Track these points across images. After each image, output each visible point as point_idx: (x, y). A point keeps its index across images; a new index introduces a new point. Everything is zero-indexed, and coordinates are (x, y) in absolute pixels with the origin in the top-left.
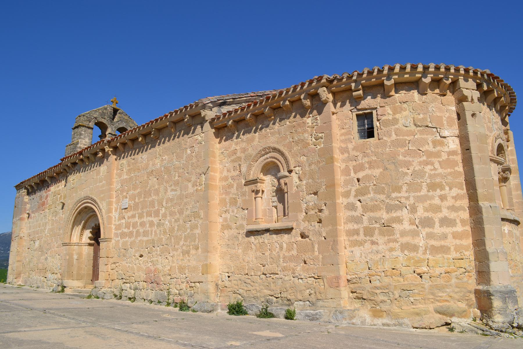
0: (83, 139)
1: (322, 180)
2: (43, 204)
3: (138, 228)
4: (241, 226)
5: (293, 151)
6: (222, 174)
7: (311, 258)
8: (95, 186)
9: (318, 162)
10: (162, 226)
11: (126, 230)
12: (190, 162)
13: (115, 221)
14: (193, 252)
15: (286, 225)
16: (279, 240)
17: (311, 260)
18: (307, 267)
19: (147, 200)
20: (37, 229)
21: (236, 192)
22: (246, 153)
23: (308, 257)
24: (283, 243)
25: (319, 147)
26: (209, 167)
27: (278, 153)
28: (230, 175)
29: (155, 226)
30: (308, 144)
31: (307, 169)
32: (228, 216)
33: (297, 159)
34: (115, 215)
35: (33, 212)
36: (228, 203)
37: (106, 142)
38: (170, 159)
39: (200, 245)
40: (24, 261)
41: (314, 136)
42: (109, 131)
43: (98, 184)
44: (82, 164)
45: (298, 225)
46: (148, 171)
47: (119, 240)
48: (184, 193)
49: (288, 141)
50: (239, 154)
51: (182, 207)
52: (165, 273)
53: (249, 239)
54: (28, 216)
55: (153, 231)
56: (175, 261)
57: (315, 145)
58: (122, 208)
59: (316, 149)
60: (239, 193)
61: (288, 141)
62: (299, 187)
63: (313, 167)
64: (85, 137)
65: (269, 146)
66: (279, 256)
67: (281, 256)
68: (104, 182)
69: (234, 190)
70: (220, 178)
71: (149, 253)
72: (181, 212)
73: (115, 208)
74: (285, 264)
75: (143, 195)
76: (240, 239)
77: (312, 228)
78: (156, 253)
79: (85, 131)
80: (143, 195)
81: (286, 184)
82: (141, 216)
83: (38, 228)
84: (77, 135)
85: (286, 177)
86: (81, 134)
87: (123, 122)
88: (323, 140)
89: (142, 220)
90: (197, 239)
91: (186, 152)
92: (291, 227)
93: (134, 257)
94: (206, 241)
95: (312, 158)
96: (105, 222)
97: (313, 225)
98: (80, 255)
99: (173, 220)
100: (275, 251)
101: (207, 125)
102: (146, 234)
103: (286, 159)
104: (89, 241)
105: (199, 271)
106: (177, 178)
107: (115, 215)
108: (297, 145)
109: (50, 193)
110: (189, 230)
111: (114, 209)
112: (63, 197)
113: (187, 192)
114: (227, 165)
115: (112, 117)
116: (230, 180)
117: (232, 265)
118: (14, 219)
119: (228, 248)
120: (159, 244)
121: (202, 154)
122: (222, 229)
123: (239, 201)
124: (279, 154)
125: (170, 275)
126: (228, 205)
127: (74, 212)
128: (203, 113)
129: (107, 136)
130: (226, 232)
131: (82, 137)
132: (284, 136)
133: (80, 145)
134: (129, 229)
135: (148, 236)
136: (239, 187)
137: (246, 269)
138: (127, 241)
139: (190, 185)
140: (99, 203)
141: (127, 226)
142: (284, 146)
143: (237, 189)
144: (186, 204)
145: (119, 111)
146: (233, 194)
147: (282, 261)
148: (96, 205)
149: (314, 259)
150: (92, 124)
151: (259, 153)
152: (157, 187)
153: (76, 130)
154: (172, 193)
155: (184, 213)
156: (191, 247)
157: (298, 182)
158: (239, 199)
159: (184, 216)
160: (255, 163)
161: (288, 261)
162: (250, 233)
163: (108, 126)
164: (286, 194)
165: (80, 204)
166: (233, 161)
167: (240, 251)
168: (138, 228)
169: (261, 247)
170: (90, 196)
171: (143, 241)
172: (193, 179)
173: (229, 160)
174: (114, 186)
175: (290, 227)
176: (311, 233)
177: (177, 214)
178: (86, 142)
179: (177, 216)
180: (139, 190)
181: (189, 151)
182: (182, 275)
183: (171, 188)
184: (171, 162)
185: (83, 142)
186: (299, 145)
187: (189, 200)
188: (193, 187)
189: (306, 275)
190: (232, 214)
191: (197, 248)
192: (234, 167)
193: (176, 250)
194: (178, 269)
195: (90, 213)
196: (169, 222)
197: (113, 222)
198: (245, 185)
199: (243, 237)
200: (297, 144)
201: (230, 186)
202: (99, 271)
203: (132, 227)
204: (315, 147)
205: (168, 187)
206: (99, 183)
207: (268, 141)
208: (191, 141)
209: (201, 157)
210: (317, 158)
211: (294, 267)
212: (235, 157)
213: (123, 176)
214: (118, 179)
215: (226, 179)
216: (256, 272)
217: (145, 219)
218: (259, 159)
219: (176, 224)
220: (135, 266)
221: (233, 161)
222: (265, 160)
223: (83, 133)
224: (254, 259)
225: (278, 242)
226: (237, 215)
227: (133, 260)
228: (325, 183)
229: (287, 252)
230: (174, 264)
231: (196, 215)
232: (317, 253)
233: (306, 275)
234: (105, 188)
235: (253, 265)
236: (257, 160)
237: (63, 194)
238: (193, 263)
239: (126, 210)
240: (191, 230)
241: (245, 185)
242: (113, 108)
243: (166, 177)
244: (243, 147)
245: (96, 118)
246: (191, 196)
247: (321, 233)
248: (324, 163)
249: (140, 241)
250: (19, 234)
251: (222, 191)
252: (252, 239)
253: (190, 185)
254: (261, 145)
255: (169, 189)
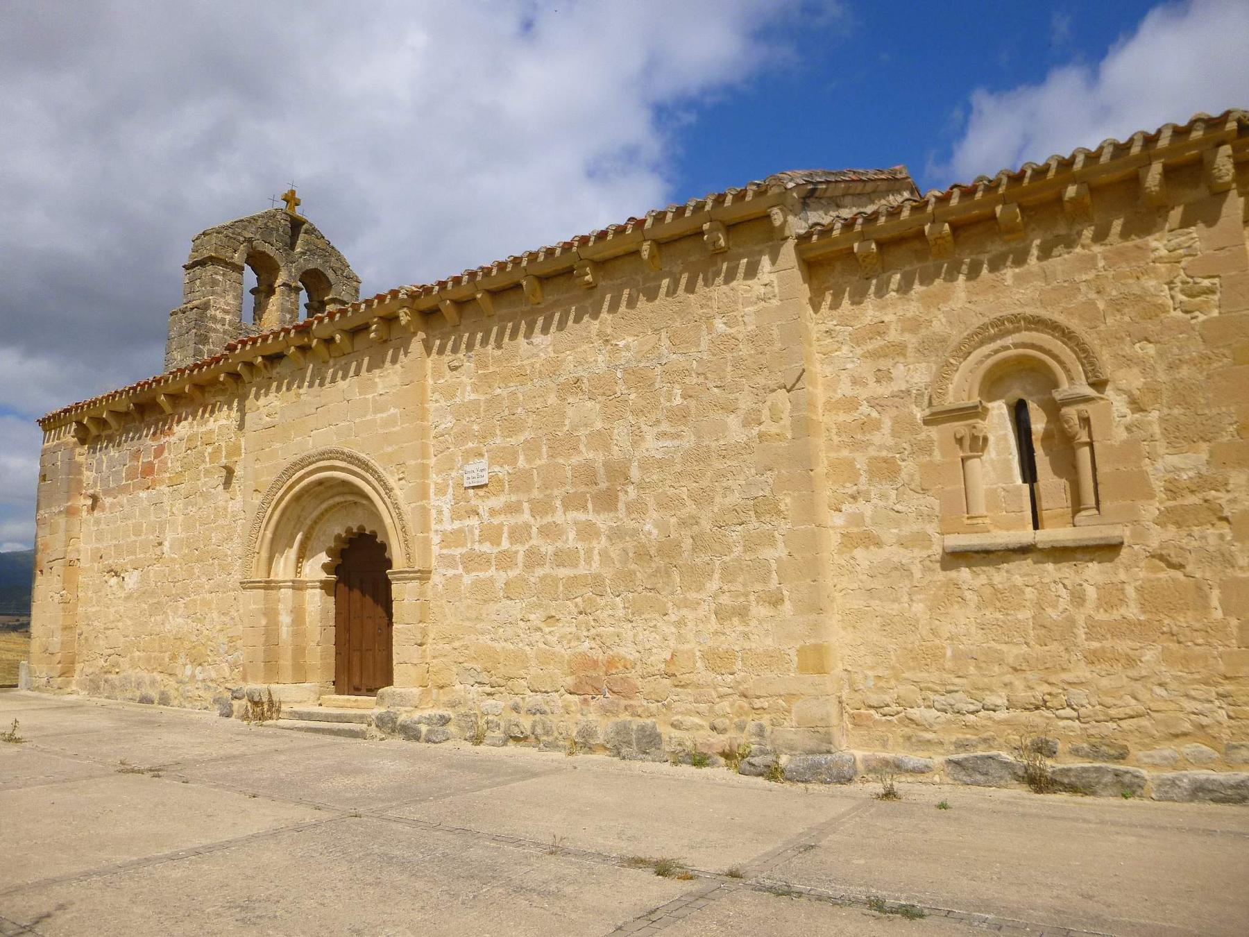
0: (222, 297)
1: (1224, 409)
2: (149, 470)
3: (534, 542)
4: (921, 540)
5: (1102, 327)
6: (835, 391)
7: (1197, 625)
8: (357, 420)
9: (1203, 357)
10: (632, 536)
11: (486, 548)
12: (729, 356)
13: (441, 521)
14: (763, 611)
15: (1098, 535)
16: (1068, 575)
17: (1195, 633)
18: (1182, 651)
19: (561, 461)
20: (129, 540)
21: (890, 441)
22: (923, 332)
23: (1185, 625)
24: (1085, 585)
25: (1202, 317)
26: (804, 370)
27: (1048, 334)
28: (864, 393)
29: (603, 539)
30: (1163, 308)
31: (1162, 376)
32: (866, 509)
33: (1122, 349)
34: (441, 503)
35: (107, 492)
36: (861, 472)
37: (405, 297)
38: (646, 348)
39: (785, 592)
40: (85, 628)
41: (1179, 284)
42: (282, 278)
43: (369, 417)
44: (302, 359)
45: (1140, 535)
46: (562, 380)
47: (461, 576)
48: (714, 444)
49: (1081, 298)
50: (893, 335)
51: (704, 483)
52: (651, 670)
53: (953, 574)
54: (89, 502)
55: (596, 552)
56: (691, 636)
57: (1186, 312)
58: (466, 485)
59: (1193, 321)
60: (905, 445)
61: (1083, 300)
62: (1134, 429)
63: (1184, 372)
64: (224, 291)
65: (1015, 312)
66: (1072, 622)
67: (1081, 620)
68: (392, 411)
69: (883, 437)
70: (828, 402)
71: (581, 613)
72: (703, 498)
73: (436, 483)
74: (1095, 645)
75: (544, 449)
76: (917, 574)
77: (1195, 544)
78: (611, 612)
79: (224, 275)
80: (544, 449)
81: (1086, 421)
82: (541, 508)
83: (133, 538)
84: (203, 284)
85: (1087, 399)
86: (214, 283)
87: (316, 257)
88: (1216, 297)
89: (549, 519)
90: (774, 575)
91: (710, 330)
92: (1120, 540)
93: (521, 623)
94: (809, 580)
95: (1180, 349)
96: (410, 524)
97: (1196, 534)
98: (298, 614)
99: (674, 520)
100: (1055, 607)
101: (788, 249)
102: (562, 558)
103: (1084, 351)
104: (323, 576)
105: (787, 666)
106: (678, 401)
107: (441, 503)
108: (1118, 311)
109: (173, 439)
110: (738, 550)
111: (432, 486)
112: (224, 453)
113: (722, 442)
114: (849, 366)
115: (289, 241)
116: (865, 408)
117: (891, 647)
118: (42, 512)
119: (872, 598)
120: (622, 588)
121: (776, 332)
122: (846, 546)
123: (908, 467)
124: (1053, 336)
125: (674, 675)
126: (863, 479)
127: (280, 494)
128: (777, 217)
129: (277, 289)
130: (859, 553)
131: (218, 289)
132: (1066, 284)
133: (213, 313)
134: (499, 544)
135: (576, 566)
136: (902, 426)
137: (944, 655)
138: (491, 580)
139: (733, 421)
140: (381, 470)
141: (491, 535)
142: (1069, 312)
143: (894, 433)
144: (720, 475)
145: (304, 227)
146: (881, 447)
147: (1084, 636)
148: (368, 476)
149: (1209, 630)
150: (238, 258)
151: (977, 334)
152: (599, 425)
153: (198, 270)
154: (660, 444)
155: (718, 499)
156: (752, 598)
157: (1131, 418)
158: (904, 460)
159: (716, 510)
160: (961, 360)
161: (1109, 636)
162: (956, 558)
163: (282, 264)
164: (1087, 449)
165: (302, 472)
166: (873, 355)
167: (919, 608)
168: (534, 542)
169: (1000, 596)
170: (346, 450)
171: (556, 580)
172: (745, 402)
173: (859, 351)
174: (428, 421)
175: (1114, 542)
176: (1191, 558)
177: (688, 502)
178: (228, 304)
179: (688, 510)
180: (527, 435)
181: (721, 325)
182: (719, 677)
183: (655, 429)
184: (652, 357)
185: (219, 303)
186: (1126, 310)
187: (735, 463)
188: (744, 426)
189: (1180, 674)
190: (881, 503)
191: (776, 601)
192: (879, 370)
193: (694, 605)
194: (703, 657)
195: (332, 497)
196: (656, 526)
197: (434, 527)
198: (926, 422)
199: (926, 569)
200: (1118, 307)
201: (867, 425)
202: (394, 662)
203: (510, 538)
204: (1188, 316)
205: (643, 426)
206: (375, 412)
207: (1007, 300)
208: (727, 296)
209: (770, 342)
210: (1196, 348)
211: (1131, 652)
212: (878, 343)
213: (463, 394)
214: (443, 403)
215: (850, 404)
216: (983, 665)
217: (559, 517)
218: (975, 349)
219: (687, 533)
220: (527, 648)
221: (873, 355)
222: (996, 352)
223: (220, 278)
224: (973, 630)
225: (1066, 582)
226: (898, 507)
227: (520, 632)
228: (1235, 419)
229: (1102, 610)
230: (687, 647)
231: (764, 508)
232: (1219, 614)
233: (1180, 674)
234: (397, 429)
235: (971, 647)
236: (970, 353)
237: (223, 444)
238: (763, 642)
239: (481, 492)
240: (747, 549)
241: (926, 422)
242: (291, 216)
243: (632, 396)
244: (909, 315)
245: (250, 241)
246: (743, 452)
247: (1230, 558)
248: (1225, 360)
249: (542, 579)
250: (66, 552)
251: (836, 439)
252: (964, 574)
253: (733, 421)
254: (978, 309)
255: (650, 434)
